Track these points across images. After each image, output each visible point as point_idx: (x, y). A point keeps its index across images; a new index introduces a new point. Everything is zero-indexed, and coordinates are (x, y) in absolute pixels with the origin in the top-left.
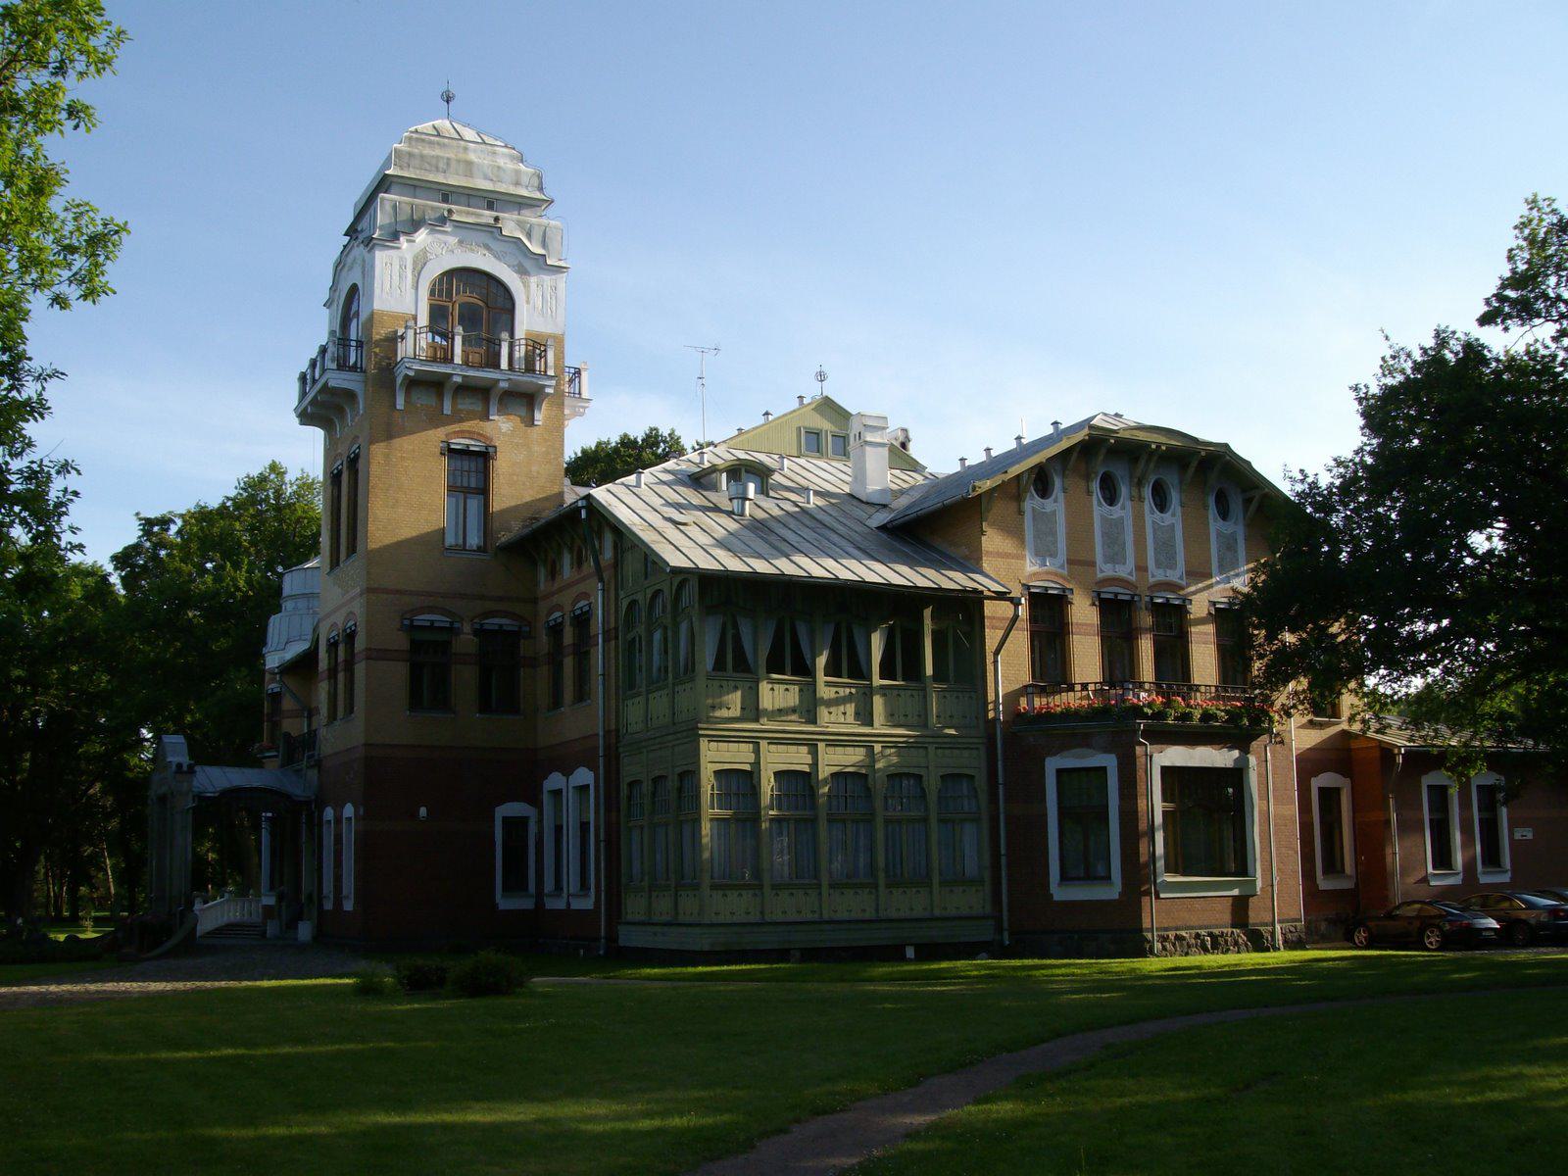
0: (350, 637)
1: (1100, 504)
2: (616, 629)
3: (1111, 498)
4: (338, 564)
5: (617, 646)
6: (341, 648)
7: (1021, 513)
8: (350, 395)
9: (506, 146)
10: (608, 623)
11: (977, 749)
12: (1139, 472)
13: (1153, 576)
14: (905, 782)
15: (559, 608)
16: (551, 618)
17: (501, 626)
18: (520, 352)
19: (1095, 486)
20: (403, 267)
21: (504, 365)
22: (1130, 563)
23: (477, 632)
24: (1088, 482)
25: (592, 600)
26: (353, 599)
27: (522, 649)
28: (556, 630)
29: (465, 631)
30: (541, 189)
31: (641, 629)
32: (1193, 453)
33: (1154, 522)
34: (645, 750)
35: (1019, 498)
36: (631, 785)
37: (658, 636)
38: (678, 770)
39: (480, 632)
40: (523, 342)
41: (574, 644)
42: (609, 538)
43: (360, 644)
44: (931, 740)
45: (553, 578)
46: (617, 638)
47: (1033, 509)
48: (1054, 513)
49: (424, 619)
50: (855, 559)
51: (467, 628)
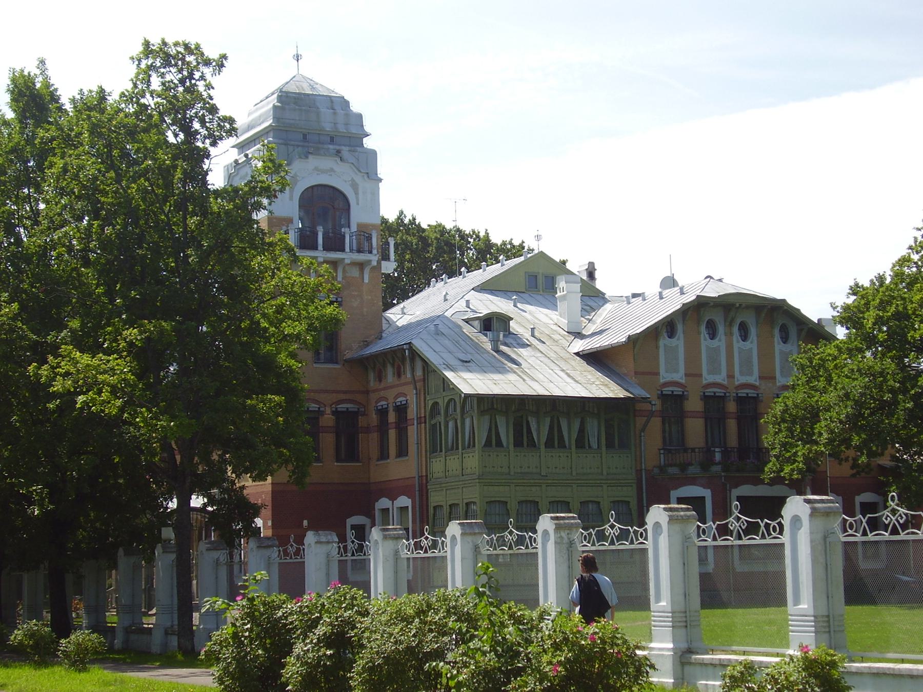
2: (425, 417)
3: (713, 335)
5: (425, 428)
7: (657, 347)
10: (420, 413)
11: (631, 486)
13: (738, 380)
14: (590, 506)
16: (379, 404)
19: (703, 328)
22: (724, 373)
23: (334, 413)
24: (698, 327)
25: (408, 397)
27: (360, 424)
28: (383, 413)
29: (327, 413)
31: (441, 418)
33: (739, 348)
34: (444, 489)
36: (435, 508)
37: (451, 424)
38: (465, 501)
39: (336, 413)
41: (396, 422)
42: (419, 365)
44: (604, 482)
45: (380, 381)
46: (425, 423)
47: (665, 345)
48: (677, 346)
51: (328, 411)
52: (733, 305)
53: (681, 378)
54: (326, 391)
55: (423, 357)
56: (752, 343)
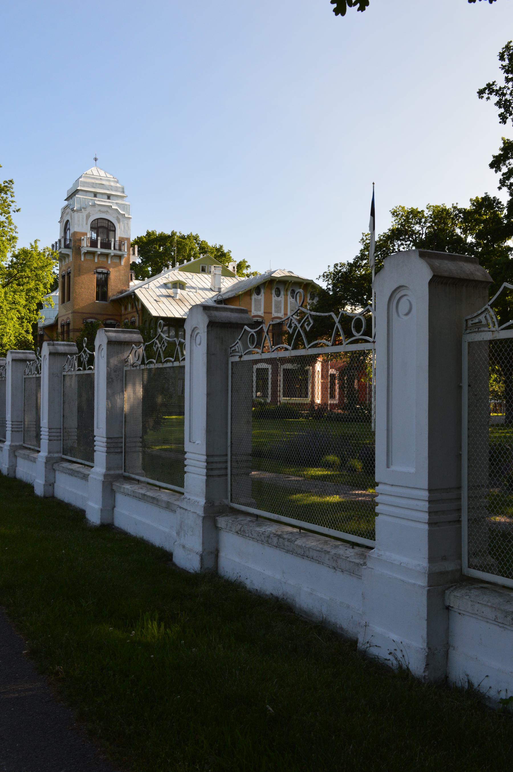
0: (68, 324)
1: (274, 297)
3: (278, 295)
4: (64, 302)
6: (65, 327)
7: (251, 299)
8: (68, 255)
9: (113, 178)
12: (287, 287)
15: (127, 319)
17: (111, 323)
18: (117, 243)
19: (273, 292)
20: (83, 218)
21: (112, 248)
25: (136, 318)
26: (69, 314)
30: (123, 192)
32: (303, 283)
35: (251, 295)
40: (118, 241)
43: (71, 327)
45: (126, 310)
47: (255, 299)
48: (261, 299)
49: (90, 320)
50: (15, 470)
52: (288, 281)
53: (262, 314)
54: (100, 314)
55: (391, 364)
56: (281, 297)
